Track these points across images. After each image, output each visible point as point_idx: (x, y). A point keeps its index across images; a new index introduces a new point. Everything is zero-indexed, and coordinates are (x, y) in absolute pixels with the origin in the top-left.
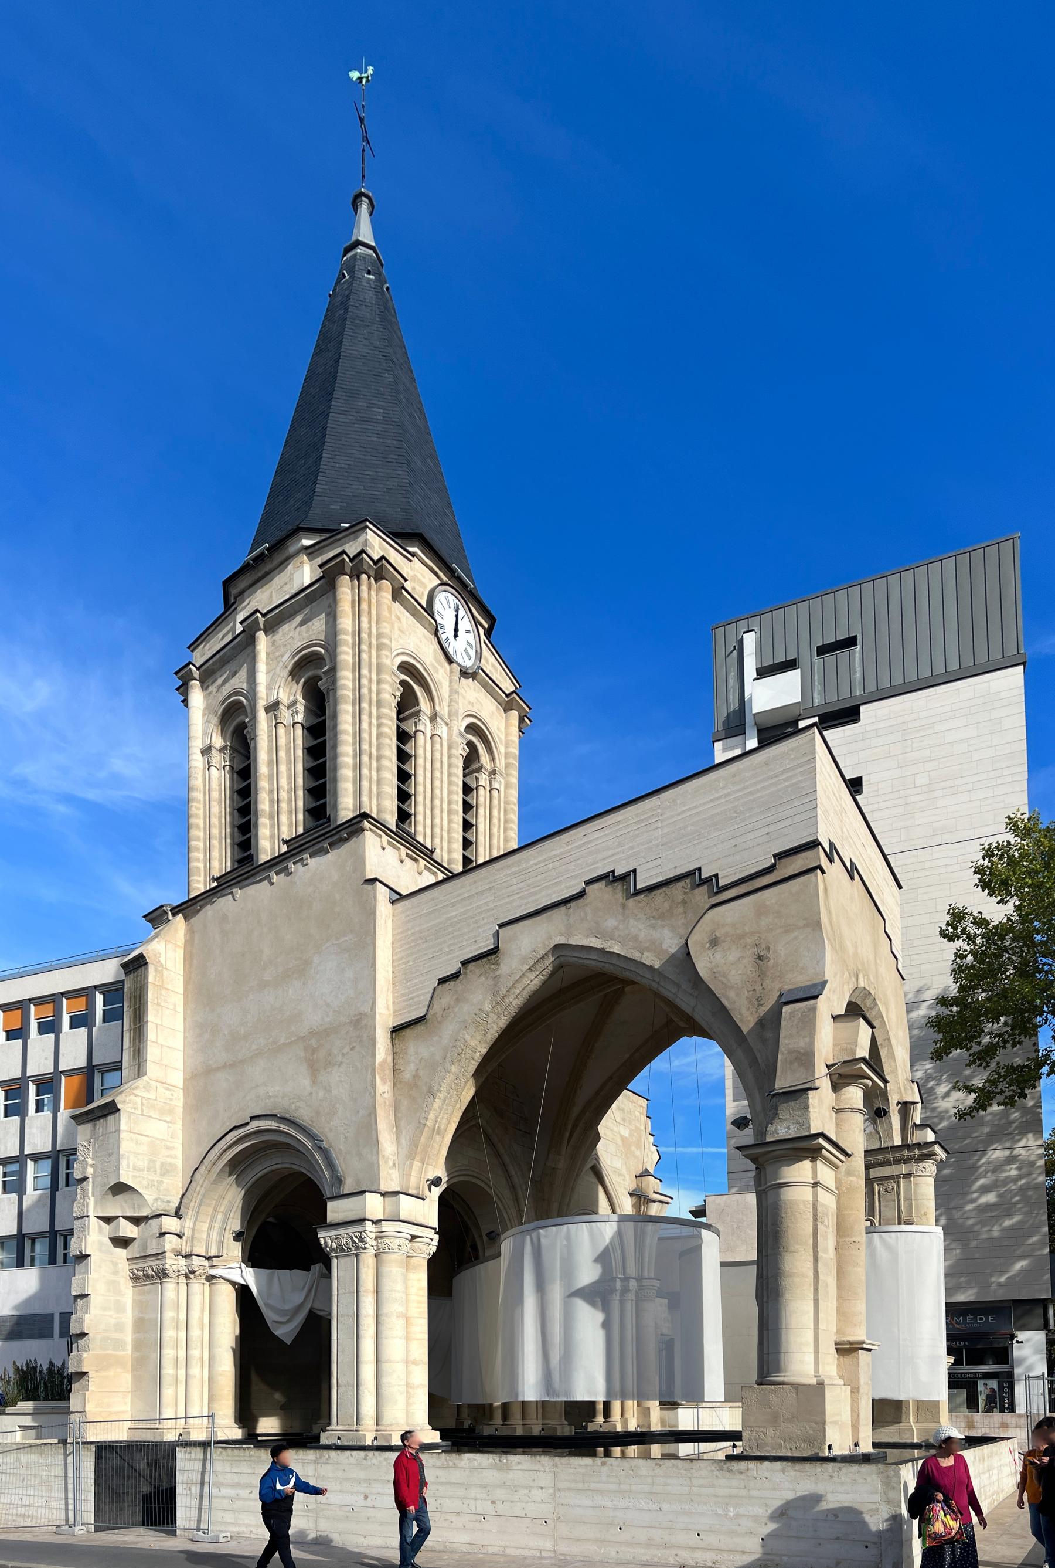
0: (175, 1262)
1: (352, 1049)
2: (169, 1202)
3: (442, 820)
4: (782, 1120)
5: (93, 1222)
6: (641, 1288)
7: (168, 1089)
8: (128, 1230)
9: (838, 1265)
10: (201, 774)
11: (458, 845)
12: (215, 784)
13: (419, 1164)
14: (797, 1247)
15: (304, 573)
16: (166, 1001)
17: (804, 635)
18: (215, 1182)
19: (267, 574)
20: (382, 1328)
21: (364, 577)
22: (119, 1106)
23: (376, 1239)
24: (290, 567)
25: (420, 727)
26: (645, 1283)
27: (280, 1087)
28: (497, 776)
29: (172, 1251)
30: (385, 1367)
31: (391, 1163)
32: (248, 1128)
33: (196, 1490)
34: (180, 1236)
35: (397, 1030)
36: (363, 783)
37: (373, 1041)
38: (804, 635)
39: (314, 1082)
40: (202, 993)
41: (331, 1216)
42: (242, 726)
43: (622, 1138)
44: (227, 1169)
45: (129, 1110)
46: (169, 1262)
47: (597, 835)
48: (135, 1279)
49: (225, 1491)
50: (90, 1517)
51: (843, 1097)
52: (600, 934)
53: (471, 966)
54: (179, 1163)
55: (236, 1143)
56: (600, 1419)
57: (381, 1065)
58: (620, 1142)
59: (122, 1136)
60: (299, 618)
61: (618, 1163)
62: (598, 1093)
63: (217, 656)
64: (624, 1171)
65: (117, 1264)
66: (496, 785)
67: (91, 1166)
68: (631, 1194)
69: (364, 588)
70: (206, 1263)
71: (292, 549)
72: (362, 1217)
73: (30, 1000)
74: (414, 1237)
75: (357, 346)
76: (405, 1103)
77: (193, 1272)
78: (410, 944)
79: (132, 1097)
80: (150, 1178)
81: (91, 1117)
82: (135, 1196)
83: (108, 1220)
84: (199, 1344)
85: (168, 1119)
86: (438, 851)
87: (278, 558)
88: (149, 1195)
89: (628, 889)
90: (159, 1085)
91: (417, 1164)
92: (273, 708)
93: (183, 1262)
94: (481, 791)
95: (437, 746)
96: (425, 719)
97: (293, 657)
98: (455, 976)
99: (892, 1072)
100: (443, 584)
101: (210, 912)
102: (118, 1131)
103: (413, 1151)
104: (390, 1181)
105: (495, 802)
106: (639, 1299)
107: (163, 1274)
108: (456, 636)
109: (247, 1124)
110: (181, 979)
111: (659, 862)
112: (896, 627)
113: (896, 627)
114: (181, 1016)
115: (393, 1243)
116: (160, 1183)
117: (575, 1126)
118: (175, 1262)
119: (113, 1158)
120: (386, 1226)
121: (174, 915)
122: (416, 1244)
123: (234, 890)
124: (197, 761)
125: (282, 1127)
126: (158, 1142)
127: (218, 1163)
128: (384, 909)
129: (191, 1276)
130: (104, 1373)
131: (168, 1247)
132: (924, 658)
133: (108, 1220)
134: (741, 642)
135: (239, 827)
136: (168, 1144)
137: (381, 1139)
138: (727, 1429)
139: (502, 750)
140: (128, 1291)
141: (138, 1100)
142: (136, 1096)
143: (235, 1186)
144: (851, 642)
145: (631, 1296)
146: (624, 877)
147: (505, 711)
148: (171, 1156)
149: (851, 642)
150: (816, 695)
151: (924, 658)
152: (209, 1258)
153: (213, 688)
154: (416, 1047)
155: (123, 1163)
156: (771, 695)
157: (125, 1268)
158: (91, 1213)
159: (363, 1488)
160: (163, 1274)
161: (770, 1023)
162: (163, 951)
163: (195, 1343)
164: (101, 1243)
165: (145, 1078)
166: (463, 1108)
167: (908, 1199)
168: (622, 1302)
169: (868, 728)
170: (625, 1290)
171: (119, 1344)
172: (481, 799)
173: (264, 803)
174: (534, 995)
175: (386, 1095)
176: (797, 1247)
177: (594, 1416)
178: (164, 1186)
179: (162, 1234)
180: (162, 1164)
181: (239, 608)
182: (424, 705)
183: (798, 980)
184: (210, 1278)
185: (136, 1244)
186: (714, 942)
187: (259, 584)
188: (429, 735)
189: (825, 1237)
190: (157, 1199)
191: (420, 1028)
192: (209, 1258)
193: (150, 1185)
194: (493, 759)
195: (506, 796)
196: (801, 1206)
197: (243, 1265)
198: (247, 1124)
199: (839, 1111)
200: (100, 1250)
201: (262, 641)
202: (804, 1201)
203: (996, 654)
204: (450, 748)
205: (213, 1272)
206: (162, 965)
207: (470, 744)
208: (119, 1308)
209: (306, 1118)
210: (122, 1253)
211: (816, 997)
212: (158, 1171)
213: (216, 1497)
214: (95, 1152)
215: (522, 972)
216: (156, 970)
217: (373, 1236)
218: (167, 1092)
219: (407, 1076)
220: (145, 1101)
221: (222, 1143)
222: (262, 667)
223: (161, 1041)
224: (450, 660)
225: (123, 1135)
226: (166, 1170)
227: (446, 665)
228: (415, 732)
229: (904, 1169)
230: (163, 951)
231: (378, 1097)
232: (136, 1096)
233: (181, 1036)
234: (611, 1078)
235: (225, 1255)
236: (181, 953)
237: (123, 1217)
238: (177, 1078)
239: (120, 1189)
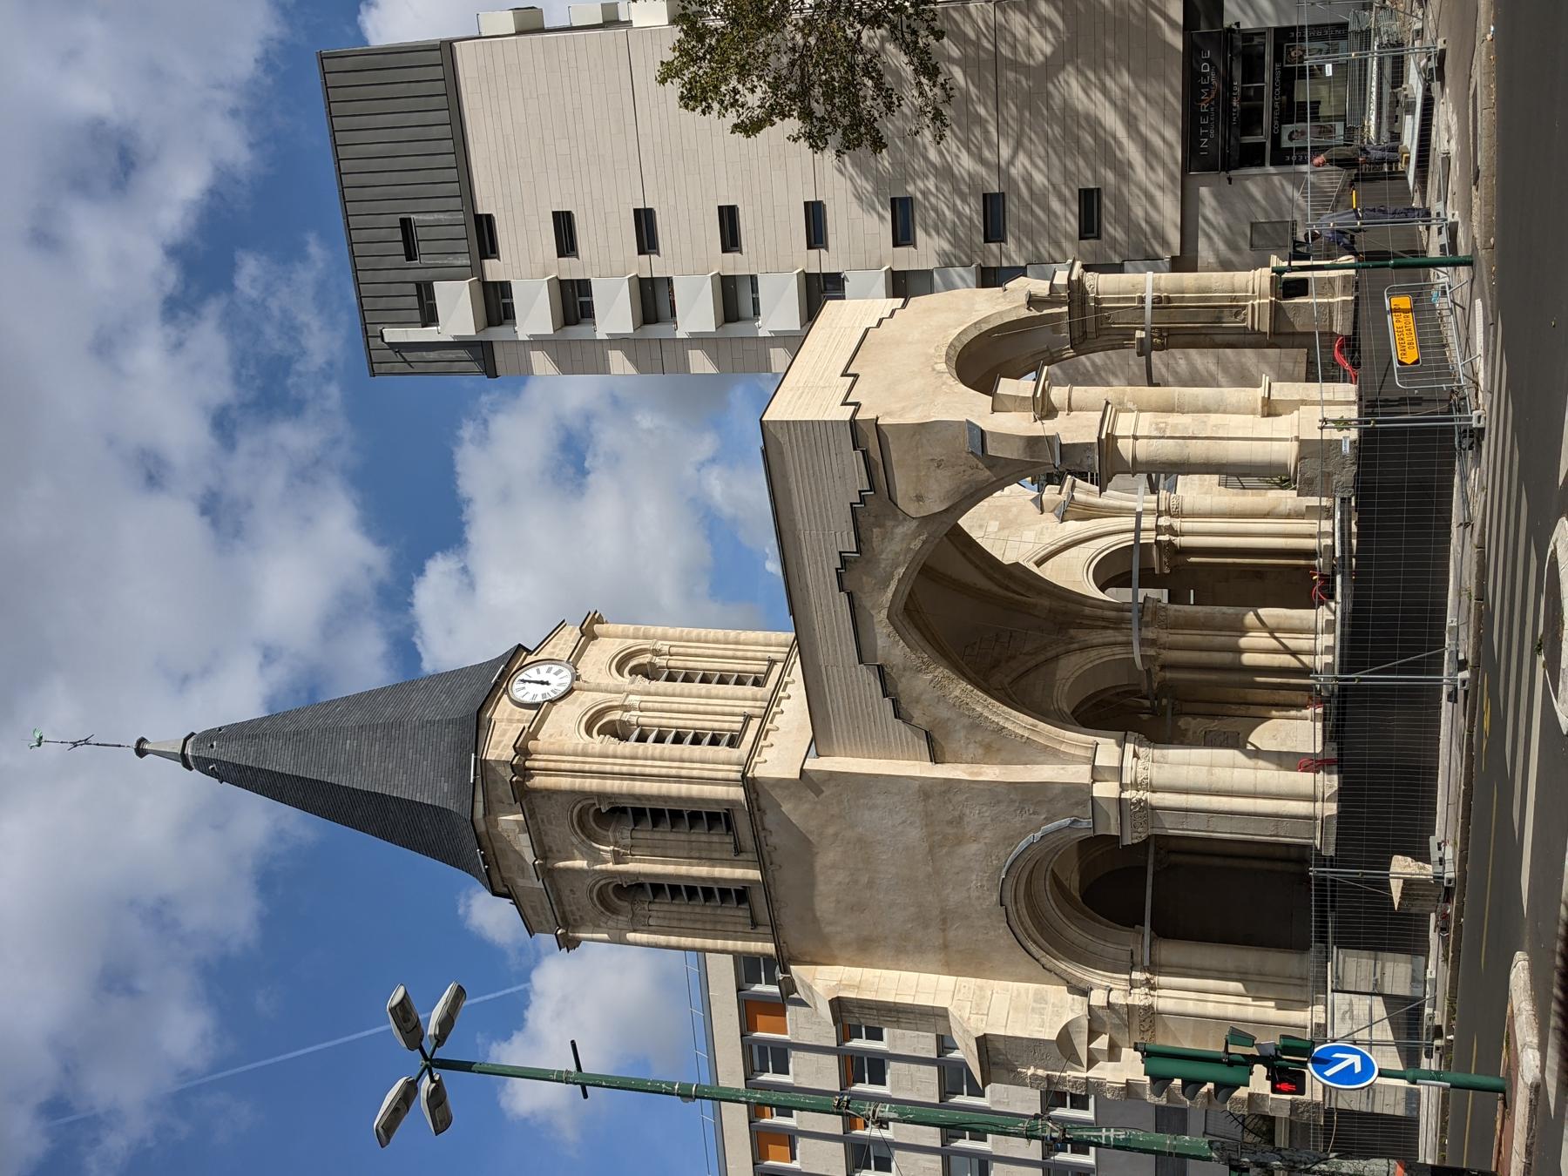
3: (716, 705)
5: (1091, 1074)
6: (1168, 512)
8: (1102, 1043)
9: (1199, 412)
11: (740, 690)
15: (511, 820)
17: (393, 275)
21: (528, 764)
25: (634, 720)
26: (1162, 508)
30: (1260, 788)
36: (707, 777)
37: (949, 783)
38: (393, 275)
40: (865, 950)
41: (1114, 831)
42: (618, 888)
43: (1001, 528)
53: (890, 689)
54: (1033, 986)
58: (1006, 532)
61: (1029, 535)
62: (977, 567)
64: (1038, 527)
68: (1063, 521)
69: (536, 764)
75: (283, 762)
89: (856, 559)
94: (672, 663)
96: (626, 716)
98: (895, 703)
100: (506, 690)
103: (1051, 754)
105: (681, 650)
106: (1180, 514)
112: (395, 178)
113: (395, 178)
114: (885, 972)
117: (1007, 588)
120: (1127, 779)
132: (432, 147)
134: (392, 345)
135: (706, 900)
139: (630, 642)
144: (406, 225)
145: (1177, 523)
146: (844, 561)
149: (406, 225)
150: (459, 263)
151: (432, 147)
156: (457, 312)
161: (992, 463)
164: (1114, 1069)
165: (951, 1009)
167: (1118, 300)
168: (1183, 534)
169: (500, 205)
170: (1170, 530)
172: (679, 664)
182: (616, 715)
183: (964, 443)
185: (1115, 1036)
186: (919, 498)
189: (1175, 426)
193: (1058, 1014)
194: (643, 651)
199: (1070, 409)
203: (438, 72)
207: (633, 671)
214: (1023, 1066)
215: (889, 644)
224: (570, 691)
226: (1040, 999)
234: (964, 554)
237: (1089, 1042)
238: (948, 981)
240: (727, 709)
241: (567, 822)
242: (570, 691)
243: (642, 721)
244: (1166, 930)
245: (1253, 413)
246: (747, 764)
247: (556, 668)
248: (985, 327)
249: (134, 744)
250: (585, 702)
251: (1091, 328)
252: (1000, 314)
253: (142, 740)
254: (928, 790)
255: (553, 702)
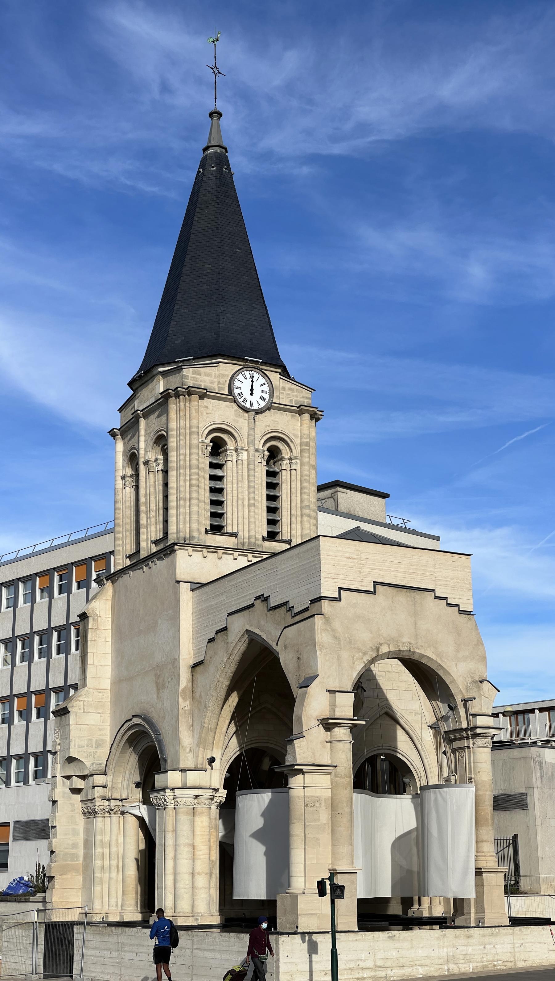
0: (102, 804)
1: (172, 679)
2: (101, 764)
4: (289, 754)
5: (59, 779)
7: (100, 692)
8: (79, 783)
10: (121, 492)
12: (128, 495)
13: (203, 750)
14: (295, 821)
16: (99, 637)
18: (121, 752)
19: (146, 382)
20: (177, 853)
22: (70, 709)
23: (174, 799)
24: (155, 380)
27: (146, 698)
28: (294, 461)
29: (99, 797)
30: (178, 877)
31: (188, 750)
32: (132, 722)
33: (81, 950)
34: (105, 787)
35: (195, 666)
39: (158, 697)
44: (127, 744)
45: (76, 711)
46: (97, 804)
47: (258, 572)
48: (85, 814)
49: (92, 952)
50: (41, 969)
51: (333, 734)
52: (259, 627)
55: (129, 729)
56: (416, 907)
57: (183, 690)
59: (71, 728)
60: (157, 413)
63: (126, 426)
65: (74, 805)
66: (294, 467)
67: (59, 744)
70: (121, 804)
71: (155, 372)
72: (163, 787)
73: (91, 558)
74: (197, 796)
76: (196, 711)
77: (112, 810)
78: (201, 614)
79: (78, 702)
80: (89, 751)
81: (59, 714)
82: (80, 763)
83: (68, 778)
84: (116, 857)
85: (100, 712)
86: (240, 533)
87: (150, 375)
88: (87, 762)
90: (94, 691)
91: (201, 749)
92: (146, 463)
93: (107, 803)
95: (240, 467)
97: (155, 435)
99: (453, 682)
100: (245, 367)
101: (125, 579)
102: (69, 724)
104: (186, 761)
105: (294, 478)
107: (95, 812)
108: (252, 394)
109: (131, 720)
110: (110, 620)
111: (277, 594)
115: (181, 801)
116: (95, 753)
118: (102, 804)
119: (67, 741)
120: (177, 792)
121: (107, 580)
122: (199, 800)
123: (130, 572)
124: (120, 483)
125: (144, 724)
126: (94, 727)
127: (122, 742)
128: (186, 597)
129: (111, 812)
130: (64, 877)
131: (96, 795)
133: (68, 778)
136: (100, 727)
137: (181, 736)
138: (135, 920)
140: (81, 820)
141: (82, 703)
142: (80, 701)
143: (134, 754)
147: (300, 415)
148: (103, 735)
152: (121, 800)
153: (126, 440)
154: (202, 679)
155: (72, 744)
157: (79, 807)
158: (58, 775)
159: (135, 949)
160: (95, 812)
162: (98, 607)
163: (114, 856)
164: (64, 793)
165: (86, 688)
166: (232, 710)
171: (75, 857)
173: (143, 520)
174: (245, 654)
175: (186, 708)
176: (295, 821)
177: (412, 905)
178: (98, 754)
179: (94, 787)
180: (96, 740)
181: (137, 396)
182: (231, 445)
183: (311, 674)
184: (123, 813)
185: (84, 791)
187: (144, 386)
188: (234, 461)
190: (93, 764)
191: (202, 667)
192: (121, 800)
195: (301, 472)
196: (297, 799)
197: (141, 804)
198: (131, 720)
200: (63, 797)
201: (142, 422)
202: (298, 797)
204: (248, 465)
205: (123, 809)
206: (97, 615)
208: (75, 833)
209: (155, 719)
210: (78, 797)
211: (308, 686)
212: (94, 746)
213: (87, 955)
215: (239, 625)
216: (94, 620)
217: (172, 797)
218: (100, 694)
219: (197, 695)
220: (85, 703)
221: (123, 729)
222: (142, 439)
223: (96, 663)
224: (246, 410)
225: (72, 727)
226: (99, 744)
227: (246, 415)
228: (226, 462)
229: (465, 743)
230: (98, 607)
231: (180, 711)
232: (80, 701)
233: (109, 657)
235: (130, 798)
236: (110, 603)
238: (107, 684)
239: (71, 760)
240: (240, 520)
241: (157, 428)
242: (246, 410)
243: (229, 464)
244: (390, 793)
245: (332, 864)
246: (187, 544)
247: (266, 396)
248: (440, 673)
249: (219, 109)
250: (239, 423)
251: (457, 744)
252: (454, 681)
253: (220, 115)
254: (175, 662)
255: (235, 401)
